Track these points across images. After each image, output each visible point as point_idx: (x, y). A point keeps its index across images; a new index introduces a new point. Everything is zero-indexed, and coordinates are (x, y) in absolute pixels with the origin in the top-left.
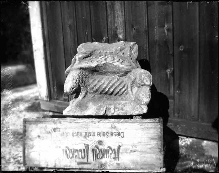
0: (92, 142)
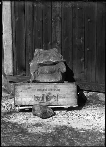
0: (46, 93)
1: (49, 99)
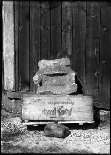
0: (58, 106)
1: (61, 114)
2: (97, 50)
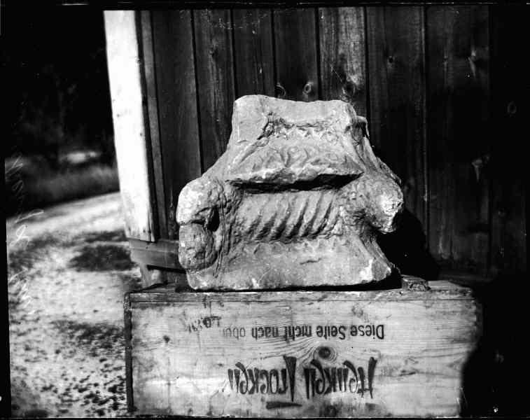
1: (321, 385)
2: (477, 54)
